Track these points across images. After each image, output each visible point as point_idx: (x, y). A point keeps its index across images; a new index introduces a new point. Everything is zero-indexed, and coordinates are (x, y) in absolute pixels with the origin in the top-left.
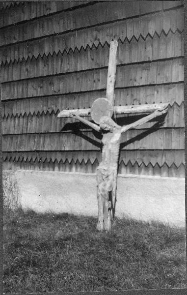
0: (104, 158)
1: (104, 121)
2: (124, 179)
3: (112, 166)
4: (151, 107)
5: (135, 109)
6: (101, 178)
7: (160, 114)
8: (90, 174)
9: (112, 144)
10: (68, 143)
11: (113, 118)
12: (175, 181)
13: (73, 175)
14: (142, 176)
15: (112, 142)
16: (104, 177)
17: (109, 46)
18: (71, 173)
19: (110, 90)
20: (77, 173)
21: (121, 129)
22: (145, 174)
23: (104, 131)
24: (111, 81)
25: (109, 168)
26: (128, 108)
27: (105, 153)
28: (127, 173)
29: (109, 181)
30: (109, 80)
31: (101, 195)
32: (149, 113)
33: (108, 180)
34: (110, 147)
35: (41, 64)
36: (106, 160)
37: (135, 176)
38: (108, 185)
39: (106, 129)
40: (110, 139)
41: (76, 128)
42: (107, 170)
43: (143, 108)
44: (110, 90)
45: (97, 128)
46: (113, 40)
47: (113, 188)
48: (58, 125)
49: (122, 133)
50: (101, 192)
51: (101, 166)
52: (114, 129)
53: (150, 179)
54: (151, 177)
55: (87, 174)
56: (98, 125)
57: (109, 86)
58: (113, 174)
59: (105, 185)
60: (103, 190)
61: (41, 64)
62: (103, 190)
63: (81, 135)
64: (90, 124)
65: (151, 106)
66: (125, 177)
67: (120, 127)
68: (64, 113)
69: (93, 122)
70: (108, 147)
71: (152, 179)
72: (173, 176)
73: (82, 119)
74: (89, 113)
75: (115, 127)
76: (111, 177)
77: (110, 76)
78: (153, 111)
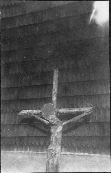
0: (52, 142)
1: (52, 118)
2: (64, 156)
3: (58, 147)
4: (83, 109)
5: (71, 111)
6: (51, 156)
7: (88, 114)
8: (40, 152)
9: (57, 133)
10: (24, 132)
11: (57, 116)
12: (98, 157)
13: (28, 153)
14: (76, 154)
15: (57, 131)
16: (53, 155)
17: (53, 71)
18: (26, 152)
19: (54, 99)
20: (30, 152)
21: (63, 123)
22: (78, 152)
23: (51, 125)
24: (55, 93)
25: (55, 149)
26: (67, 110)
27: (52, 139)
28: (66, 151)
29: (56, 158)
30: (54, 92)
31: (51, 167)
32: (78, 114)
33: (56, 157)
34: (56, 134)
35: (13, 4)
36: (53, 143)
37: (72, 153)
38: (55, 161)
39: (53, 123)
40: (56, 130)
41: (31, 122)
42: (55, 150)
43: (76, 110)
44: (54, 99)
45: (47, 122)
46: (55, 69)
47: (58, 163)
48: (80, 116)
49: (63, 126)
50: (51, 165)
51: (51, 148)
52: (58, 123)
53: (82, 156)
54: (82, 154)
55: (38, 153)
56: (48, 121)
57: (54, 96)
58: (59, 152)
59: (53, 161)
60: (52, 164)
61: (13, 4)
62: (52, 164)
63: (34, 127)
64: (41, 119)
65: (81, 109)
66: (65, 155)
67: (61, 122)
68: (24, 112)
69: (43, 118)
70: (54, 135)
71: (83, 156)
72: (97, 154)
73: (36, 116)
74: (41, 113)
75: (59, 122)
76: (57, 155)
77: (54, 90)
78: (84, 112)
